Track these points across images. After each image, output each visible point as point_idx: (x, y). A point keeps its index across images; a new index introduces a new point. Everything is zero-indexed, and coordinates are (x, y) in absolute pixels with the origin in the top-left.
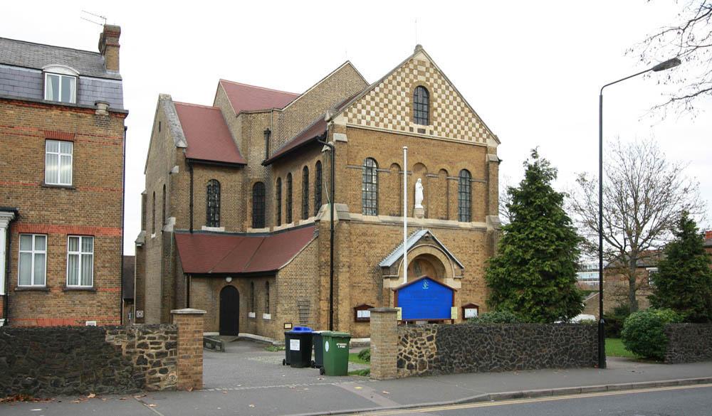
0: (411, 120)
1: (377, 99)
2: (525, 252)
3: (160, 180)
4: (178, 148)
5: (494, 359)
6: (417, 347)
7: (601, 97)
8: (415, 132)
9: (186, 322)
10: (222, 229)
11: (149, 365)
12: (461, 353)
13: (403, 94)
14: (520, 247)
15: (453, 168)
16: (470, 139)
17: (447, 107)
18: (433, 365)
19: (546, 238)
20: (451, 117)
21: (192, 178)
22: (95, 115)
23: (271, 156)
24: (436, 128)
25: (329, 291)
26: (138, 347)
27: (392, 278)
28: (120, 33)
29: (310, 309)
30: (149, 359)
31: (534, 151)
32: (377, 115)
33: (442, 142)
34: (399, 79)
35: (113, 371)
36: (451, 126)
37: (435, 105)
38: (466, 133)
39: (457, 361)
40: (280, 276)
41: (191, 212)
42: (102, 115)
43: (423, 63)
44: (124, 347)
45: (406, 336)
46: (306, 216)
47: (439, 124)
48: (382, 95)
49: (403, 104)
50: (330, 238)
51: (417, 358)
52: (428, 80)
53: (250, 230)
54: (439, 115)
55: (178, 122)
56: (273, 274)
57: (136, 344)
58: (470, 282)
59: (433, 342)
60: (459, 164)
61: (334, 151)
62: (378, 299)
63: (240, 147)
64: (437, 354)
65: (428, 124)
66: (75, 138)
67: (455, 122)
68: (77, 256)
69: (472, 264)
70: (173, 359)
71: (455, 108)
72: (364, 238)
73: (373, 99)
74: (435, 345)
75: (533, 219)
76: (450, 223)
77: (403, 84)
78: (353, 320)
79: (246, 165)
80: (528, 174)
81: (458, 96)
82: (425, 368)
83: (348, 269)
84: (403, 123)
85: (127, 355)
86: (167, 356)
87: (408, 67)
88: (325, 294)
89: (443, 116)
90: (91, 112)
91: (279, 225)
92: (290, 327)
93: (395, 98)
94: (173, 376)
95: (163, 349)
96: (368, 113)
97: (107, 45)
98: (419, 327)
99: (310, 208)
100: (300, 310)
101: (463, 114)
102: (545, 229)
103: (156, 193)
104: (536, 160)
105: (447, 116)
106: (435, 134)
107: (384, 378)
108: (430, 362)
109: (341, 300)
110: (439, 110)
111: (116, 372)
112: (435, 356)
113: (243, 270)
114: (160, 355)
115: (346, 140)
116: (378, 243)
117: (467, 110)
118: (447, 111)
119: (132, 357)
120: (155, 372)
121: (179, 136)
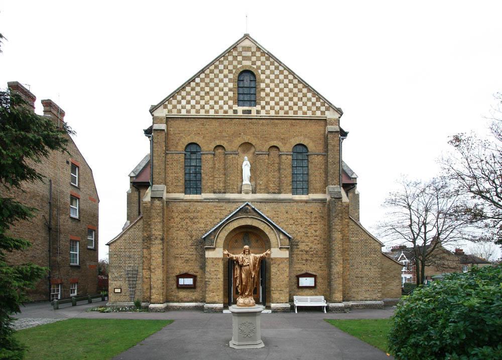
0: (234, 103)
15: (286, 144)
32: (198, 103)
33: (272, 121)
43: (248, 49)
47: (268, 103)
49: (226, 89)
52: (254, 63)
58: (307, 252)
69: (309, 235)
76: (282, 196)
92: (120, 291)
106: (263, 113)
109: (154, 269)
116: (201, 218)
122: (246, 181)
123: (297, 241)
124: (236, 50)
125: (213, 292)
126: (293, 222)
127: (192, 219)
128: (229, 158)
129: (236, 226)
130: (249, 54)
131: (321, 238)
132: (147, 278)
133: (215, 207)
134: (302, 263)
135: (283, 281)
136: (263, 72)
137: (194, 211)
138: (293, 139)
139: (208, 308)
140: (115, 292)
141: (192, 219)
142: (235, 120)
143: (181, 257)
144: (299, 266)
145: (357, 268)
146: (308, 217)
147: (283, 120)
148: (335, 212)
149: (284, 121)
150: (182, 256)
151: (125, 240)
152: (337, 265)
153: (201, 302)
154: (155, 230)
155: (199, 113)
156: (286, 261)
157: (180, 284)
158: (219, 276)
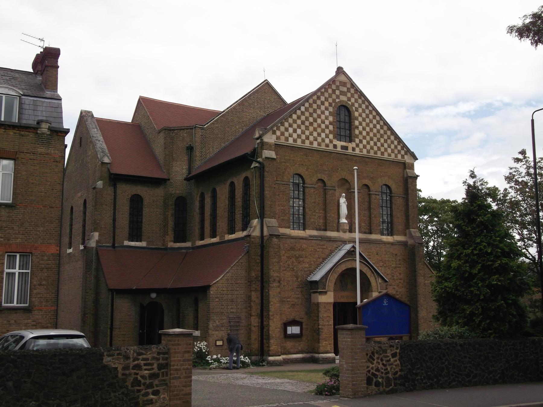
0: (334, 138)
1: (303, 118)
2: (471, 267)
3: (79, 194)
4: (103, 163)
5: (453, 375)
6: (383, 364)
7: (533, 121)
8: (339, 149)
9: (177, 342)
10: (143, 244)
11: (142, 387)
12: (422, 370)
13: (327, 113)
14: (466, 262)
16: (389, 155)
17: (368, 125)
18: (398, 382)
19: (491, 252)
20: (371, 134)
21: (115, 192)
22: (37, 133)
23: (194, 173)
24: (357, 145)
25: (259, 307)
26: (133, 369)
27: (321, 293)
28: (59, 54)
29: (241, 324)
30: (143, 381)
31: (471, 171)
32: (303, 133)
34: (323, 99)
35: (110, 394)
36: (372, 143)
37: (357, 123)
38: (386, 150)
39: (419, 378)
40: (212, 291)
41: (114, 227)
42: (43, 134)
43: (344, 84)
44: (120, 369)
45: (373, 353)
46: (232, 231)
47: (361, 141)
48: (307, 114)
49: (327, 122)
50: (260, 253)
51: (383, 375)
52: (349, 99)
53: (171, 245)
54: (361, 133)
55: (101, 138)
56: (205, 289)
57: (131, 366)
59: (397, 358)
60: (379, 180)
61: (264, 167)
62: (307, 314)
63: (162, 162)
64: (401, 370)
65: (351, 141)
66: (17, 156)
67: (375, 139)
68: (14, 274)
69: (395, 278)
70: (165, 380)
71: (375, 126)
73: (299, 118)
74: (398, 362)
75: (476, 235)
76: (374, 237)
77: (327, 104)
78: (282, 336)
79: (169, 180)
80: (468, 192)
82: (391, 385)
83: (278, 284)
84: (327, 141)
85: (123, 377)
86: (158, 377)
87: (331, 88)
88: (256, 309)
89: (364, 133)
90: (33, 130)
91: (202, 239)
92: (221, 344)
93: (319, 116)
94: (164, 398)
95: (156, 370)
96: (295, 131)
97: (46, 66)
98: (384, 343)
99: (237, 222)
100: (230, 326)
101: (382, 132)
102: (489, 244)
103: (74, 208)
104: (474, 180)
105: (368, 133)
106: (357, 151)
107: (355, 395)
108: (395, 379)
109: (273, 315)
110: (361, 128)
111: (112, 395)
112: (399, 373)
113: (169, 286)
114: (153, 376)
115: (274, 156)
116: (306, 257)
117: (385, 128)
118: (368, 129)
119: (127, 380)
120: (147, 394)
121: (103, 152)
125: (326, 341)
126: (382, 264)
127: (297, 258)
129: (344, 269)
130: (345, 89)
131: (404, 281)
132: (255, 327)
133: (317, 245)
136: (357, 110)
137: (299, 249)
138: (380, 179)
139: (323, 358)
140: (216, 345)
142: (333, 154)
143: (288, 301)
146: (394, 259)
148: (419, 257)
150: (289, 300)
151: (227, 280)
152: (422, 310)
153: (311, 353)
154: (273, 271)
155: (304, 144)
157: (288, 333)
158: (330, 323)
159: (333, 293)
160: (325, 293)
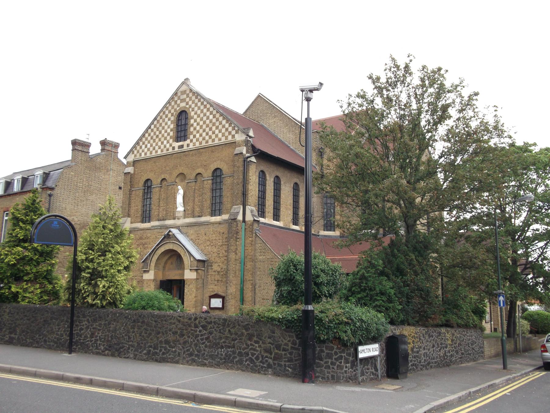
8: (176, 149)
15: (207, 170)
24: (191, 141)
33: (198, 151)
52: (187, 104)
58: (218, 272)
69: (221, 255)
72: (141, 241)
76: (203, 219)
81: (211, 106)
106: (191, 146)
116: (150, 244)
122: (180, 208)
123: (211, 262)
124: (177, 96)
128: (169, 188)
134: (214, 283)
135: (191, 301)
141: (144, 245)
142: (175, 155)
144: (212, 287)
145: (264, 289)
146: (220, 238)
147: (206, 149)
149: (207, 148)
150: (136, 278)
152: (231, 286)
156: (194, 282)
159: (153, 271)
160: (148, 271)
